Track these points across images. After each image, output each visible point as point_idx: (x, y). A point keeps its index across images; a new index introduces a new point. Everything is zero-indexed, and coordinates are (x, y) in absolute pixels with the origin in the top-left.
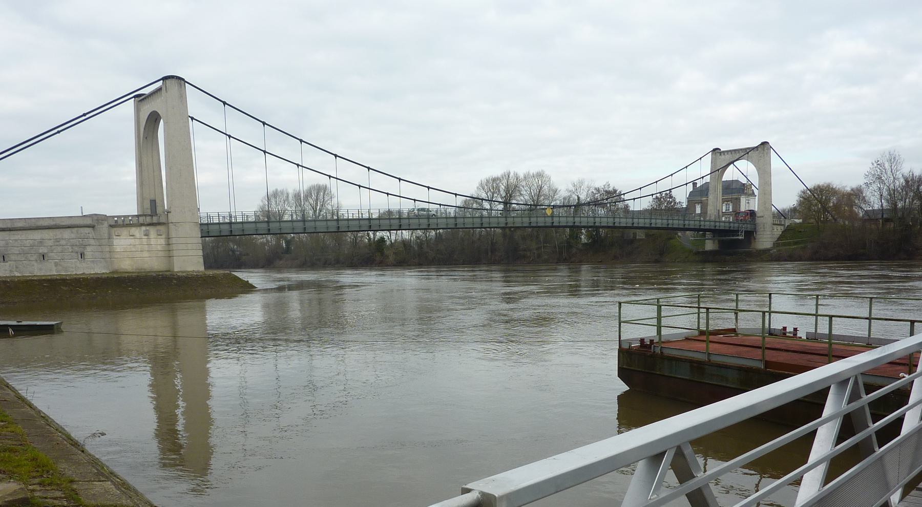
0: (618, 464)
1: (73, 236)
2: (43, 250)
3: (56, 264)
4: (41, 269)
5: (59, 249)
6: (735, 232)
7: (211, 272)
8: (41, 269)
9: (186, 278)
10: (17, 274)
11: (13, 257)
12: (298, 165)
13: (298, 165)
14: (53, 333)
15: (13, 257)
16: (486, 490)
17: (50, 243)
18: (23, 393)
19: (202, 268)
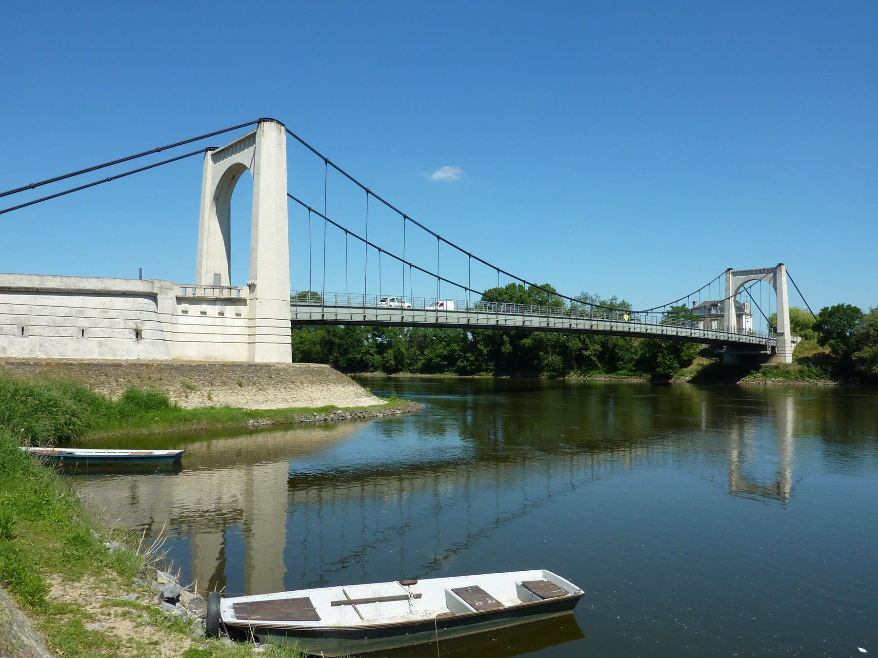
0: (780, 303)
1: (128, 306)
2: (83, 323)
3: (100, 344)
4: (77, 350)
5: (107, 323)
6: (764, 347)
7: (298, 365)
8: (77, 350)
9: (224, 365)
10: (42, 356)
11: (37, 330)
12: (466, 289)
13: (466, 289)
14: (761, 415)
15: (37, 330)
16: (817, 304)
17: (95, 313)
18: (213, 571)
19: (290, 360)
